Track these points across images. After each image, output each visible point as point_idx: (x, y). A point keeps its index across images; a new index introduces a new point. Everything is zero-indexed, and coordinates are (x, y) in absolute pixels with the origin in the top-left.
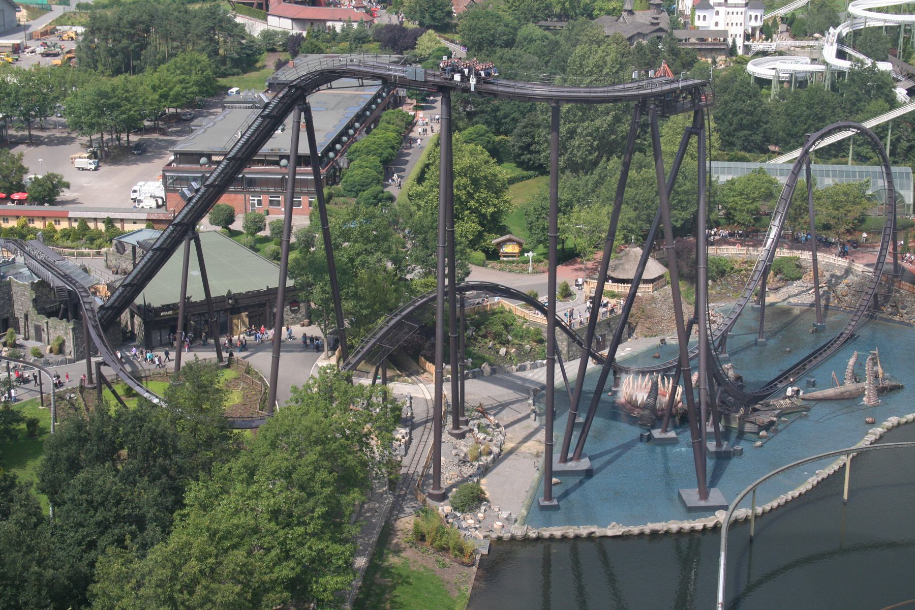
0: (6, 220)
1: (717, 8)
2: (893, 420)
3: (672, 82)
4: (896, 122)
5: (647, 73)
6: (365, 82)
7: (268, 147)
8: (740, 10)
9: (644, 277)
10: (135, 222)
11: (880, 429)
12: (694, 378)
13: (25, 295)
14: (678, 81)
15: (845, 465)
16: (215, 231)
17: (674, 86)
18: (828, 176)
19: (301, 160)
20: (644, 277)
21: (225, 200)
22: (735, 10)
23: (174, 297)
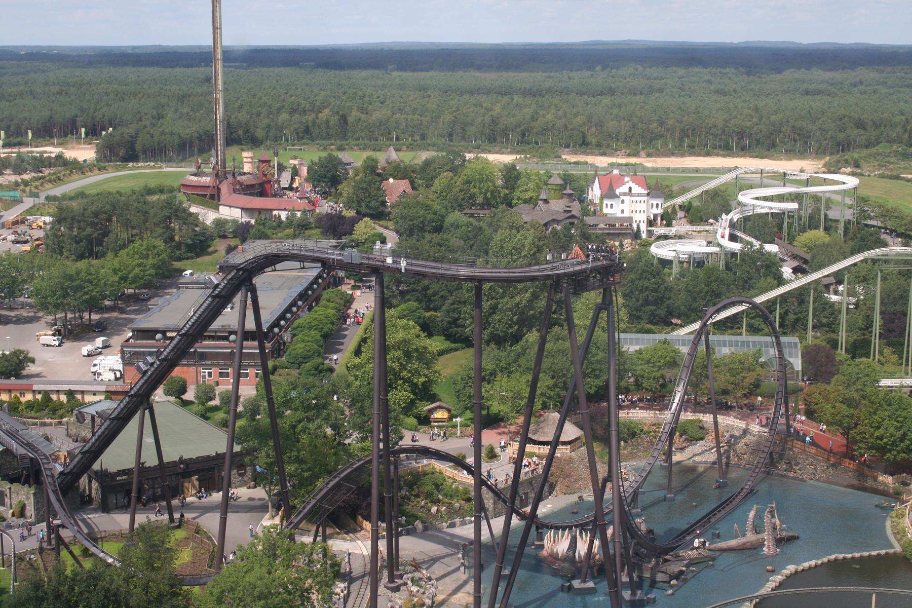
1: (622, 198)
2: (791, 568)
3: (583, 263)
4: (784, 298)
7: (217, 324)
8: (643, 199)
12: (610, 531)
16: (168, 401)
17: (584, 267)
19: (247, 335)
20: (562, 438)
21: (177, 372)
22: (638, 199)
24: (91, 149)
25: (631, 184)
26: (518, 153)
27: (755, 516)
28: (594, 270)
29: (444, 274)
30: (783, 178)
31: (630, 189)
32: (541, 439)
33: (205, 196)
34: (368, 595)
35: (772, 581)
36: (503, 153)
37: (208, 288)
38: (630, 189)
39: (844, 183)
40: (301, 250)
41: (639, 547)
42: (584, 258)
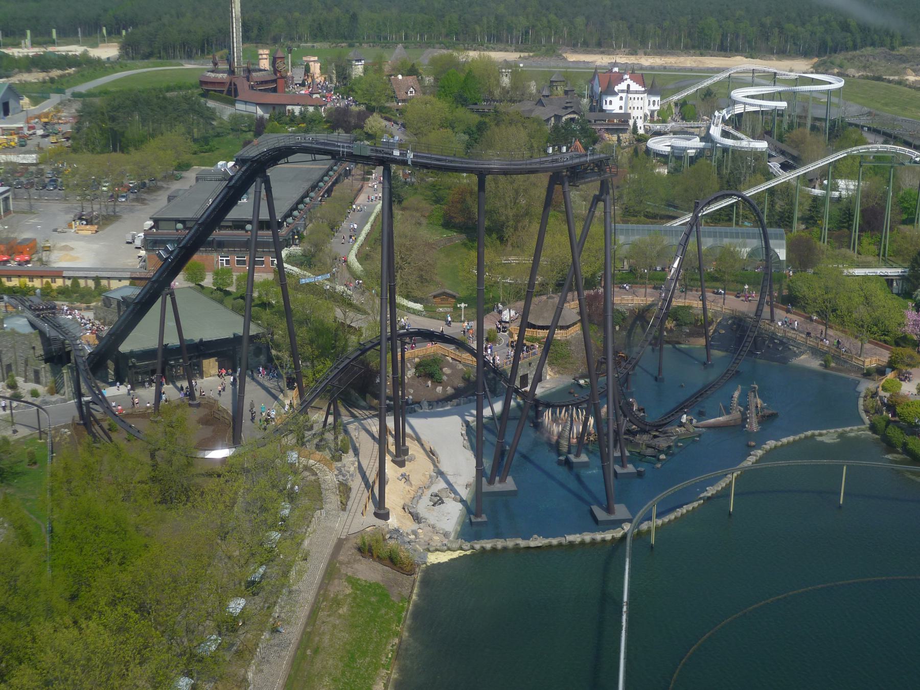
0: (9, 278)
1: (620, 95)
2: (771, 444)
3: (581, 156)
4: (771, 191)
5: (560, 149)
6: (318, 157)
7: (234, 214)
8: (640, 96)
9: (560, 324)
10: (120, 279)
11: (760, 451)
12: (604, 410)
13: (24, 344)
14: (586, 155)
15: (731, 482)
16: (189, 287)
17: (583, 159)
18: (726, 237)
19: (263, 225)
20: (560, 324)
21: (196, 257)
22: (636, 96)
23: (151, 343)
24: (115, 46)
25: (629, 82)
26: (521, 51)
27: (740, 396)
28: (592, 161)
29: (448, 166)
30: (773, 78)
31: (628, 86)
32: (541, 324)
33: (222, 92)
34: (377, 464)
35: (753, 455)
36: (507, 51)
37: (226, 180)
38: (628, 86)
39: (830, 83)
40: (311, 143)
41: (631, 424)
42: (583, 152)
